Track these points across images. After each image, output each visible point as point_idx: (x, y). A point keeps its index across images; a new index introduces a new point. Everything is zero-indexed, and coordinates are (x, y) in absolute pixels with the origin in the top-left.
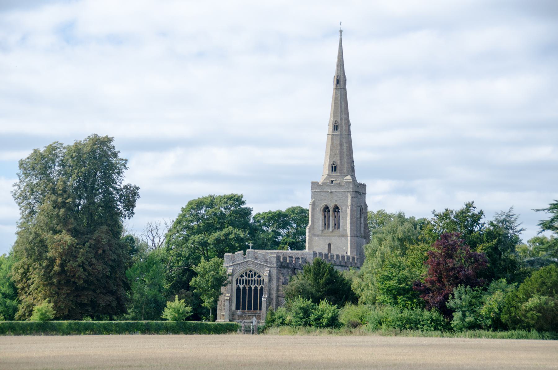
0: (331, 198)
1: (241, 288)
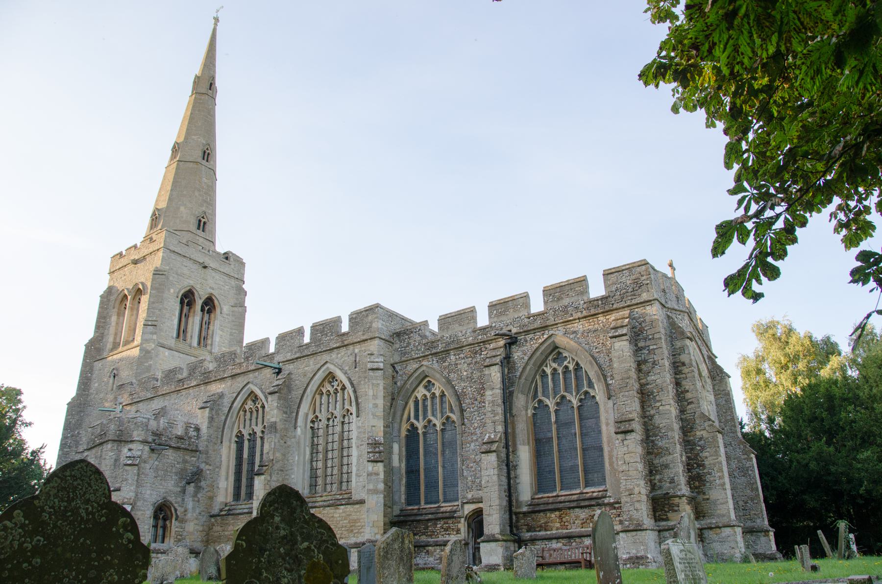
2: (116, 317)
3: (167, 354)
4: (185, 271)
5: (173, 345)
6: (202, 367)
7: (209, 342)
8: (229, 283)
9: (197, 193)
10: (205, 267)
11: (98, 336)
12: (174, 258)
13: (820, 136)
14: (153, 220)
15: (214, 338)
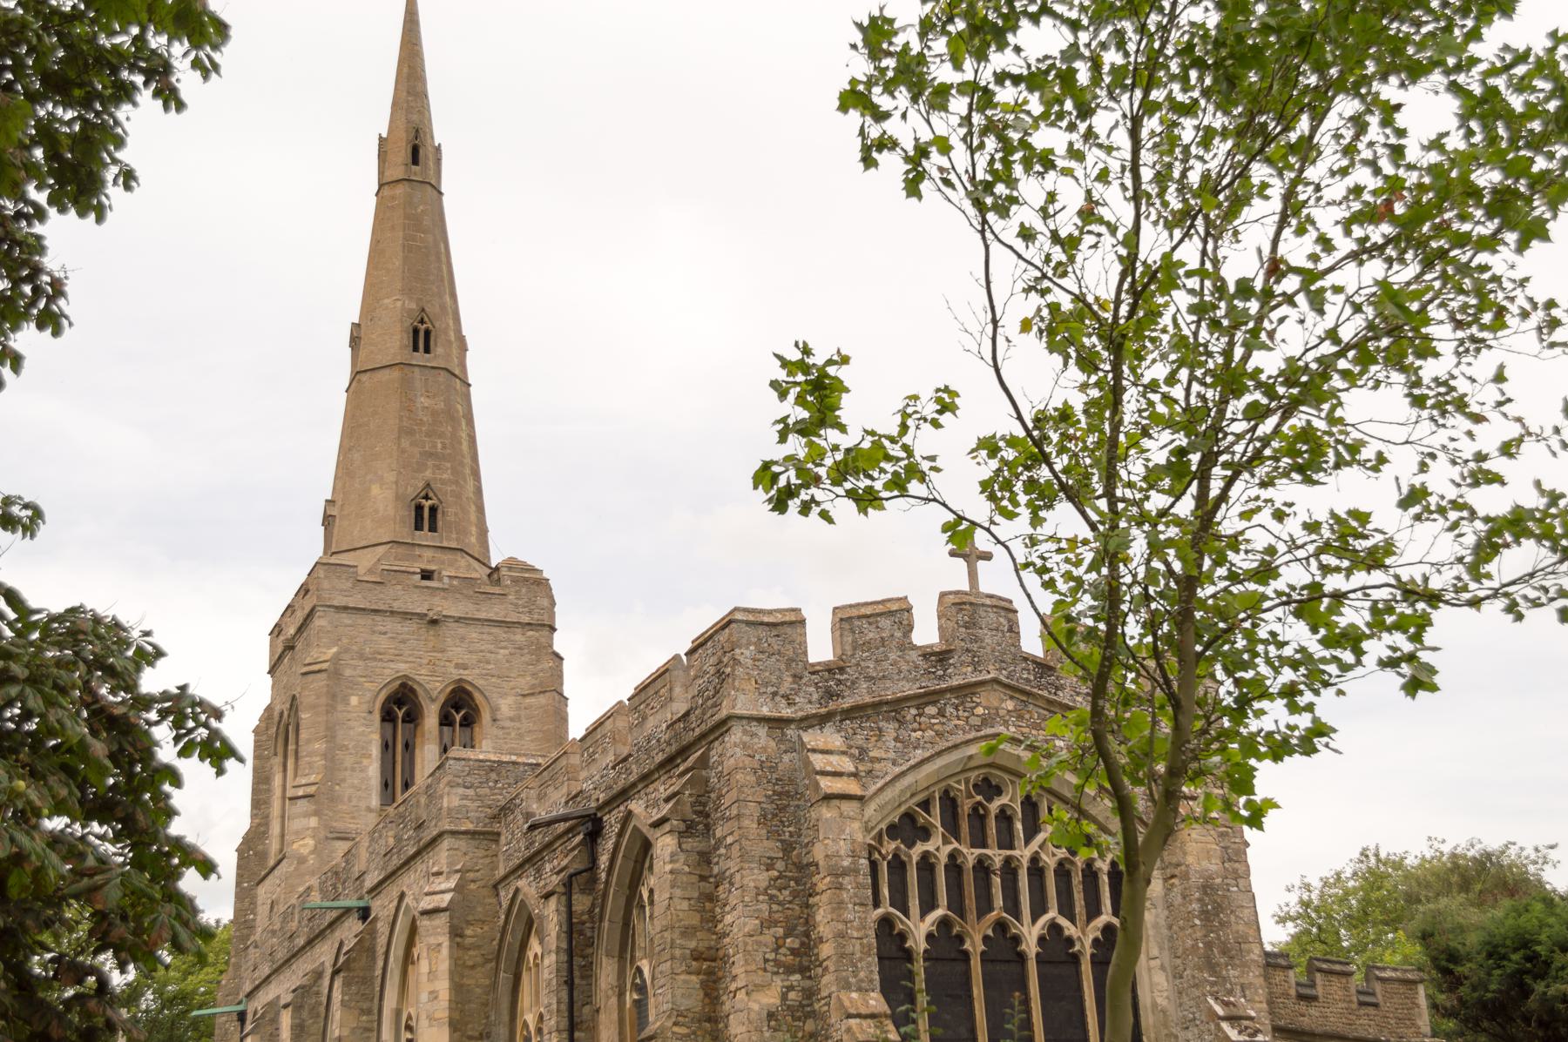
0: (434, 649)
1: (1031, 947)
4: (383, 643)
8: (509, 640)
10: (434, 622)
12: (349, 622)
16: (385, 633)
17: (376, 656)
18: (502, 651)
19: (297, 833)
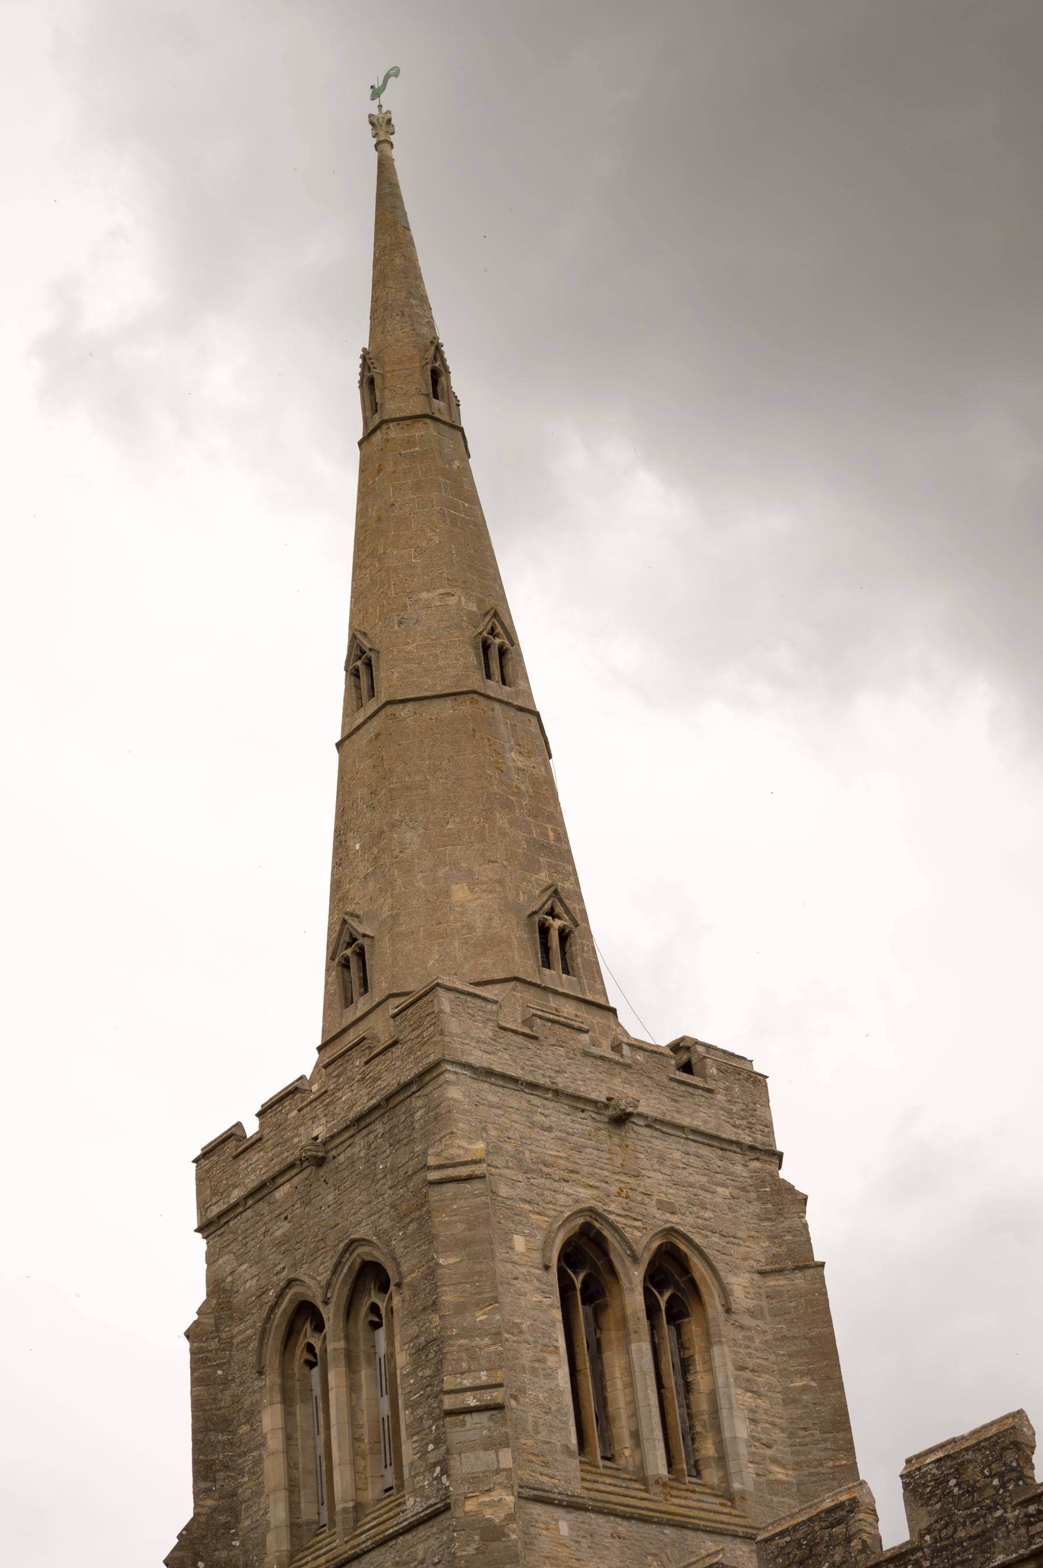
2: (278, 1408)
3: (564, 1528)
5: (577, 1488)
6: (849, 1539)
7: (708, 1448)
9: (502, 820)
11: (215, 1510)
13: (375, 868)
14: (346, 965)
15: (725, 1424)
16: (549, 1129)
17: (541, 1167)
18: (720, 1189)
19: (473, 1480)
